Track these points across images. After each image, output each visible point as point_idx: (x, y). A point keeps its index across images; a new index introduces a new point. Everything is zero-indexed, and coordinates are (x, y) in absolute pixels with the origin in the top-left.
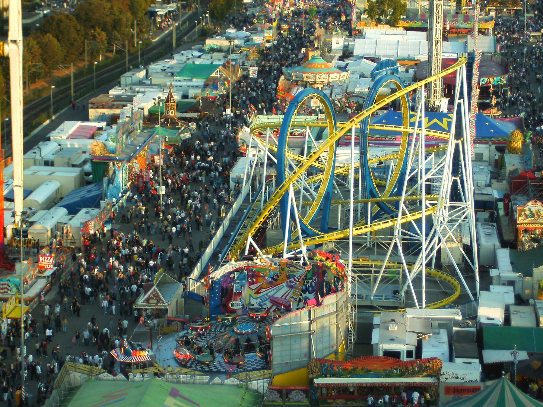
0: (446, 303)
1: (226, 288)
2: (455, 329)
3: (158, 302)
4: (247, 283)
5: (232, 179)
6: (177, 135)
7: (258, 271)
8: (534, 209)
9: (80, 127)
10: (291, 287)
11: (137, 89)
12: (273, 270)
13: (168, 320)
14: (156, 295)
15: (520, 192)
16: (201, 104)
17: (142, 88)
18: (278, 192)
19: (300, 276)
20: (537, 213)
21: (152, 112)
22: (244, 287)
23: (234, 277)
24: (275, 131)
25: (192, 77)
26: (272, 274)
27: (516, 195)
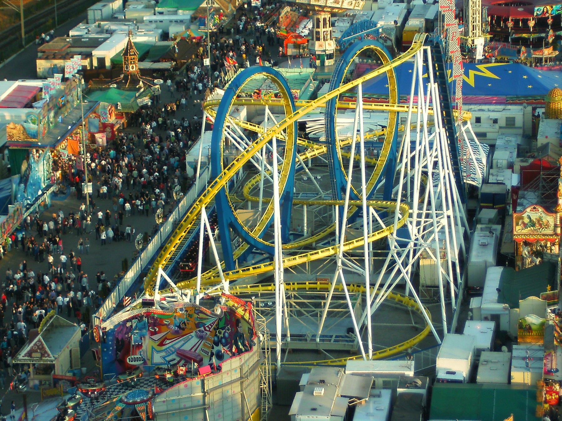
0: (408, 345)
1: (122, 340)
2: (400, 390)
3: (43, 355)
4: (148, 333)
5: (189, 163)
6: (132, 100)
7: (160, 318)
8: (534, 216)
9: (19, 88)
10: (201, 338)
11: (106, 27)
12: (179, 317)
13: (54, 379)
14: (40, 347)
15: (529, 187)
16: (177, 51)
17: (113, 25)
18: (188, 217)
19: (210, 325)
20: (538, 221)
21: (115, 63)
22: (144, 337)
23: (131, 326)
24: (255, 92)
25: (178, 8)
26: (178, 321)
27: (526, 190)
